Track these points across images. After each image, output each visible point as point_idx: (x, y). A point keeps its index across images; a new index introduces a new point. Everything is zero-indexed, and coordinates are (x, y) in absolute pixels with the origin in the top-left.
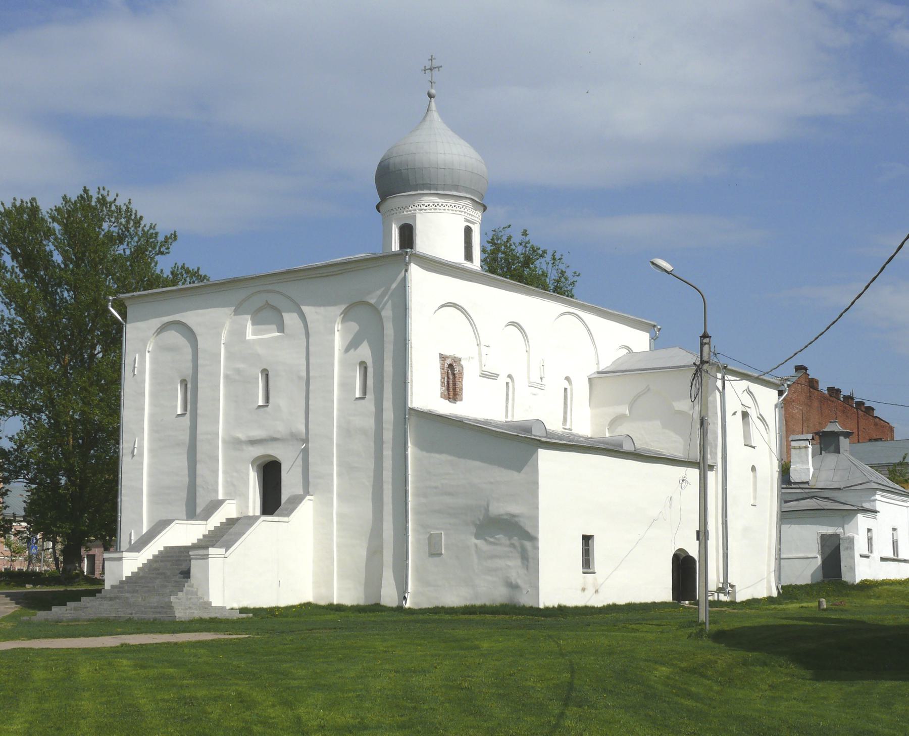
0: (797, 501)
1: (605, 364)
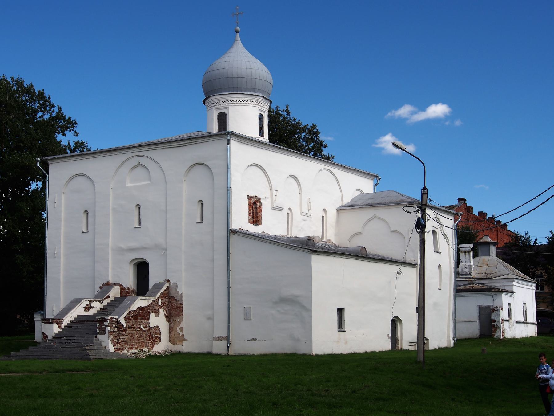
0: (465, 287)
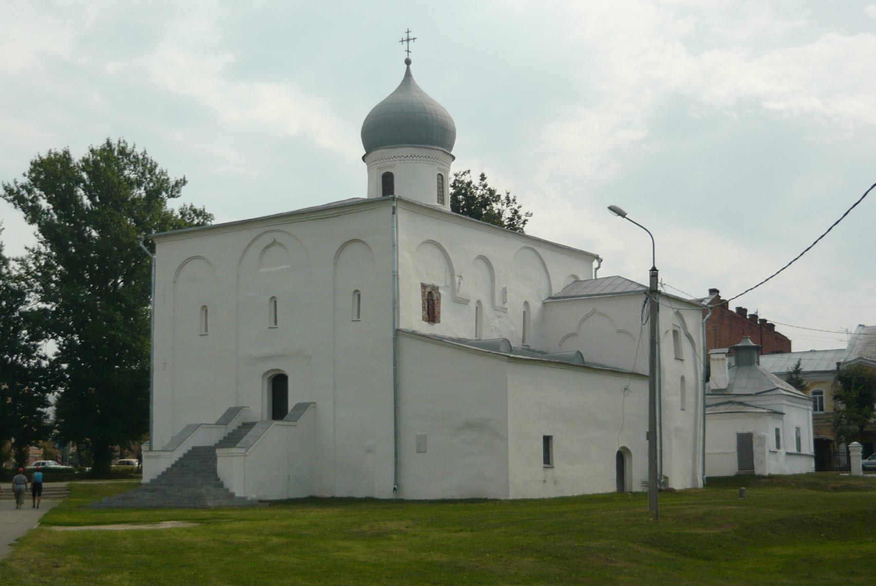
1: (556, 290)
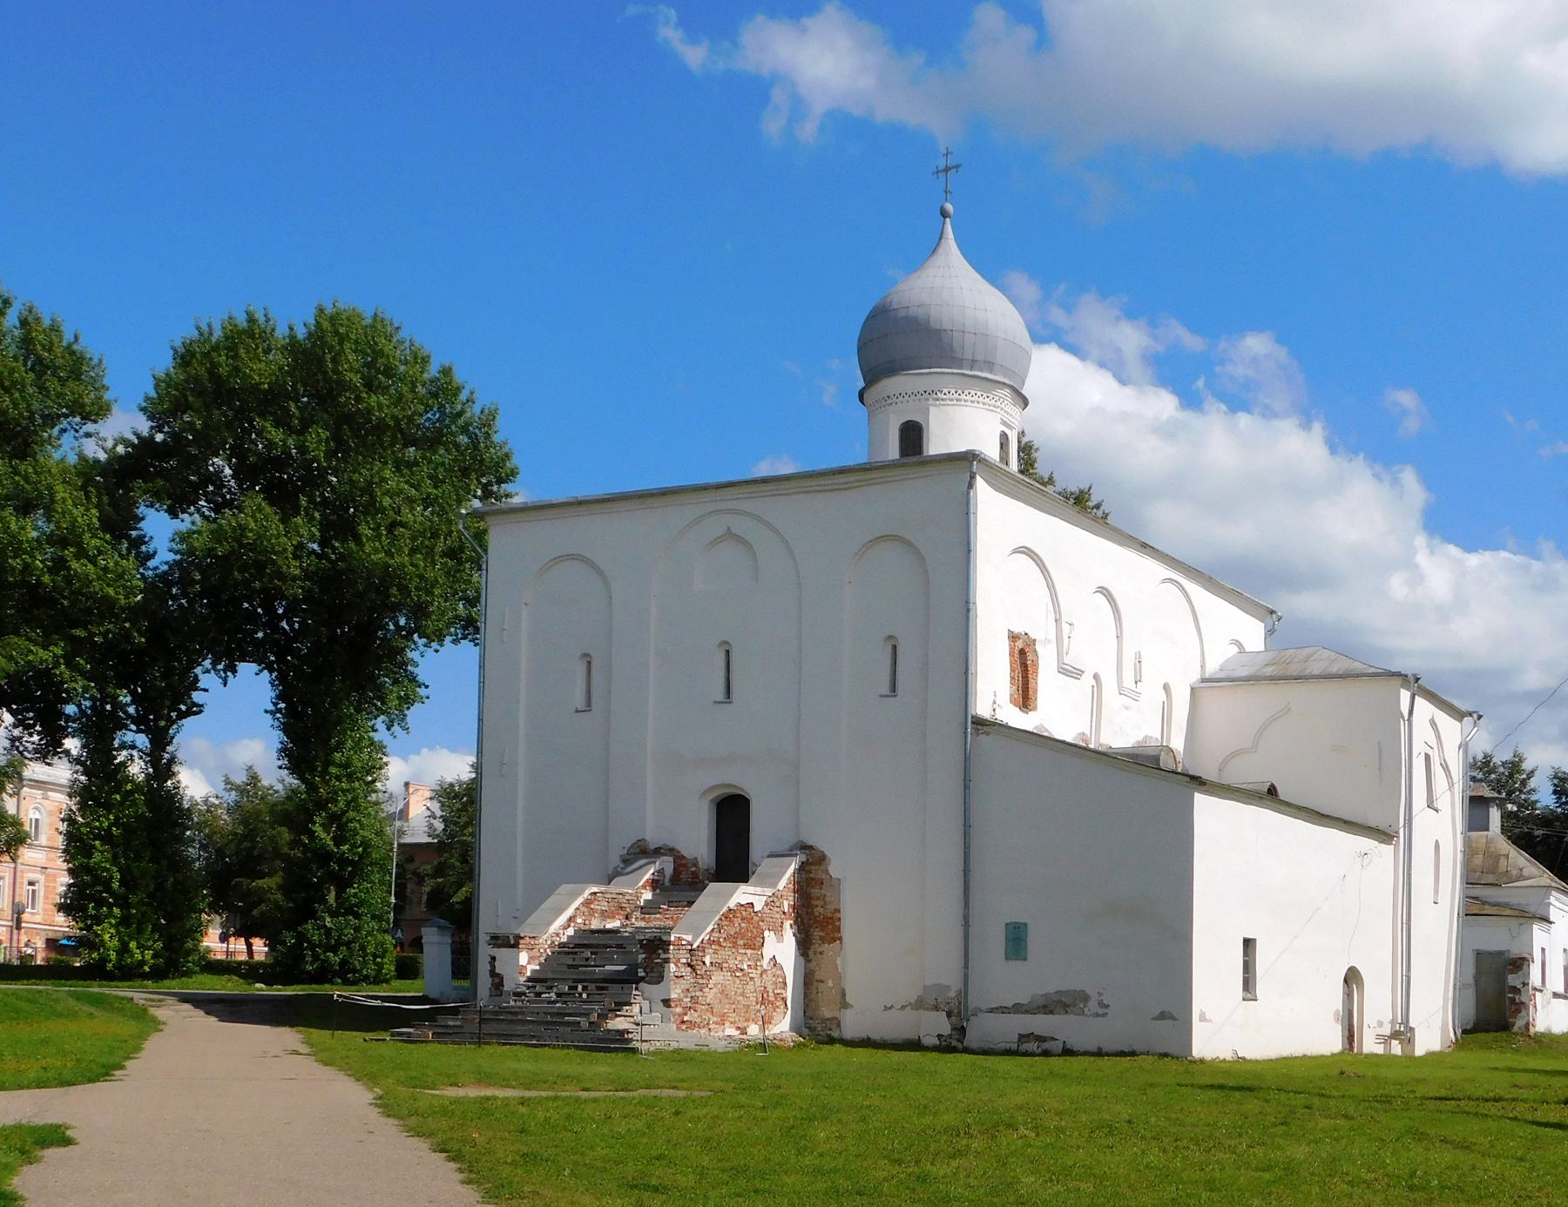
1: (1212, 667)
